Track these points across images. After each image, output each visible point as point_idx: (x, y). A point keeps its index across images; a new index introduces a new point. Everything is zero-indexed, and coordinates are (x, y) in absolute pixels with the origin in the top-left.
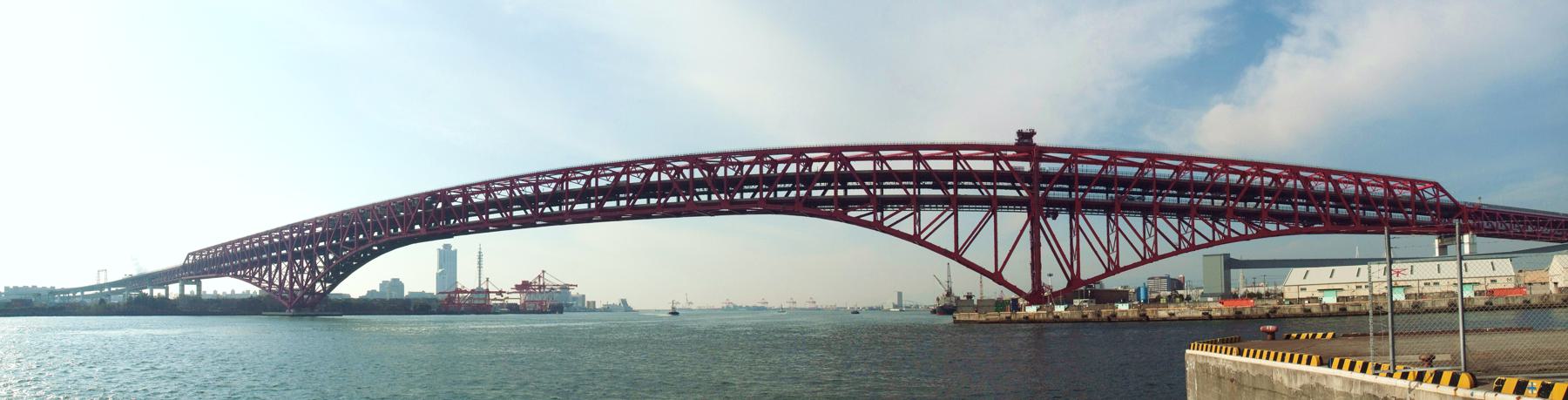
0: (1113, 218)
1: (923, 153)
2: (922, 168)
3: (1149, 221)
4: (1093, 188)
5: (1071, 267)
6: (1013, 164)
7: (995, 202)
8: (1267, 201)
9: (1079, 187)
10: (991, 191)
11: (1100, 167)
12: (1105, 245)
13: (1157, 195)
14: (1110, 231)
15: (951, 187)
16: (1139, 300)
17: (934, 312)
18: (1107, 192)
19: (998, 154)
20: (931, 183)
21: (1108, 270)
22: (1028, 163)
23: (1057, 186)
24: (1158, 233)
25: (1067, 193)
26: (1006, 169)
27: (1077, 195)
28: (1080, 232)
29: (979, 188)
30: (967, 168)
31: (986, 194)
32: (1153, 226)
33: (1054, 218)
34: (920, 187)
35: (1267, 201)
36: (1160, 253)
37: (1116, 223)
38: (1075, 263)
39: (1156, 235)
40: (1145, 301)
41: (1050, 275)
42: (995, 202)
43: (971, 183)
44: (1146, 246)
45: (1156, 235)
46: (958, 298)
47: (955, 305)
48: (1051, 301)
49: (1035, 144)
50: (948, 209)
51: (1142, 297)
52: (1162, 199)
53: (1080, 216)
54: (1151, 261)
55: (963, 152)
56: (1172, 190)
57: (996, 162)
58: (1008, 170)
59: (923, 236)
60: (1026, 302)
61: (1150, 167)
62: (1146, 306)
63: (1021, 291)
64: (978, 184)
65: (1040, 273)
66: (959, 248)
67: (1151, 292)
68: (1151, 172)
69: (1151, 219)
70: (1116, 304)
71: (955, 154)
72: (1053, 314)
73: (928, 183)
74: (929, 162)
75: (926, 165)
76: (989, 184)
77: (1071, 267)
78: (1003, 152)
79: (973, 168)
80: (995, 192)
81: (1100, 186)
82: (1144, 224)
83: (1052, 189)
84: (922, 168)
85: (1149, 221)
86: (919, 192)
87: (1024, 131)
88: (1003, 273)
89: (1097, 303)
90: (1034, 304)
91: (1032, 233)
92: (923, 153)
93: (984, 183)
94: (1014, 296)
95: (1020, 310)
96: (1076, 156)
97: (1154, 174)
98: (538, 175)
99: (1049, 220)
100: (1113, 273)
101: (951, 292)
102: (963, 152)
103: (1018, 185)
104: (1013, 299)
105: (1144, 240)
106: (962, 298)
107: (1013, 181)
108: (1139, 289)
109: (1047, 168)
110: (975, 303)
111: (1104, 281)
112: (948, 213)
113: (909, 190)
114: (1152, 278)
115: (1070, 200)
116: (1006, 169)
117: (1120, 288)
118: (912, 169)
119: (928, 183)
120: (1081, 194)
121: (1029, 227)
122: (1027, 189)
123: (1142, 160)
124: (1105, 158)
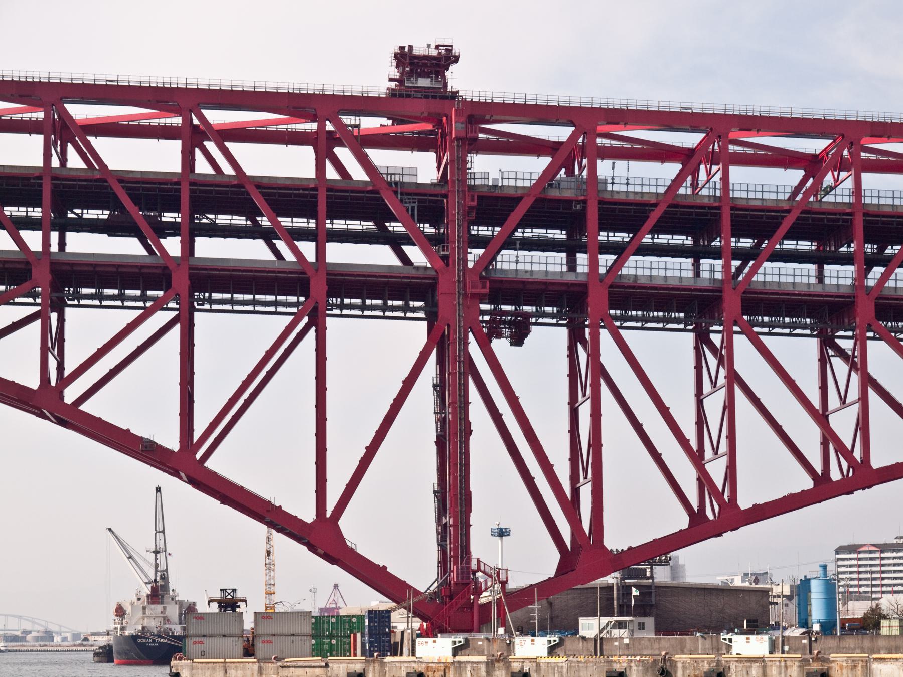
0: (716, 339)
1: (79, 112)
2: (75, 161)
3: (841, 353)
4: (647, 239)
5: (571, 507)
6: (380, 157)
7: (318, 287)
8: (607, 248)
9: (603, 236)
10: (308, 249)
11: (672, 169)
12: (690, 433)
13: (870, 263)
14: (707, 387)
15: (172, 229)
16: (804, 623)
17: (106, 655)
18: (696, 254)
19: (329, 127)
20: (104, 214)
21: (696, 516)
22: (431, 156)
23: (529, 233)
24: (872, 394)
25: (812, 268)
26: (358, 174)
27: (594, 264)
28: (605, 390)
29: (268, 236)
30: (228, 170)
31: (289, 256)
32: (853, 366)
33: (518, 340)
34: (64, 227)
35: (607, 248)
36: (877, 462)
37: (726, 358)
38: (586, 493)
39: (864, 400)
40: (828, 628)
41: (502, 533)
42: (318, 287)
43: (239, 220)
44: (829, 437)
45: (864, 400)
46: (189, 610)
47: (178, 630)
48: (503, 624)
49: (455, 94)
50: (159, 305)
51: (817, 613)
52: (885, 277)
53: (605, 335)
54: (847, 487)
55: (217, 117)
56: (789, 236)
57: (324, 154)
58: (365, 178)
59: (71, 394)
60: (417, 624)
61: (713, 159)
62: (831, 642)
63: (404, 586)
64: (265, 222)
65: (466, 526)
66: (196, 436)
67: (850, 596)
68: (848, 184)
69: (847, 344)
70: (724, 636)
71: (188, 121)
72: (508, 665)
73: (92, 214)
74: (99, 143)
75: (88, 154)
76: (300, 223)
77: (571, 507)
78: (347, 120)
79: (250, 171)
80: (320, 253)
81: (673, 233)
82: (824, 361)
83: (510, 243)
84: (75, 161)
85: (841, 353)
86: (62, 244)
87: (417, 51)
88: (344, 523)
89: (657, 632)
90: (443, 631)
91: (440, 388)
92: (79, 112)
93: (285, 221)
94: (377, 601)
95: (396, 650)
96: (592, 134)
97: (858, 190)
98: (4, 261)
99: (500, 346)
100: (716, 530)
101: (165, 587)
102: (217, 117)
103: (396, 227)
104: (374, 615)
105: (821, 417)
106: (202, 608)
107: (381, 215)
108: (806, 582)
109: (494, 175)
110: (248, 624)
111: (683, 555)
112: (161, 318)
113: (25, 234)
114: (853, 548)
115: (571, 278)
116: (358, 174)
117: (738, 583)
118: (39, 163)
119: (92, 214)
120: (606, 260)
121: (431, 368)
122: (429, 243)
123: (689, 140)
124: (689, 140)
